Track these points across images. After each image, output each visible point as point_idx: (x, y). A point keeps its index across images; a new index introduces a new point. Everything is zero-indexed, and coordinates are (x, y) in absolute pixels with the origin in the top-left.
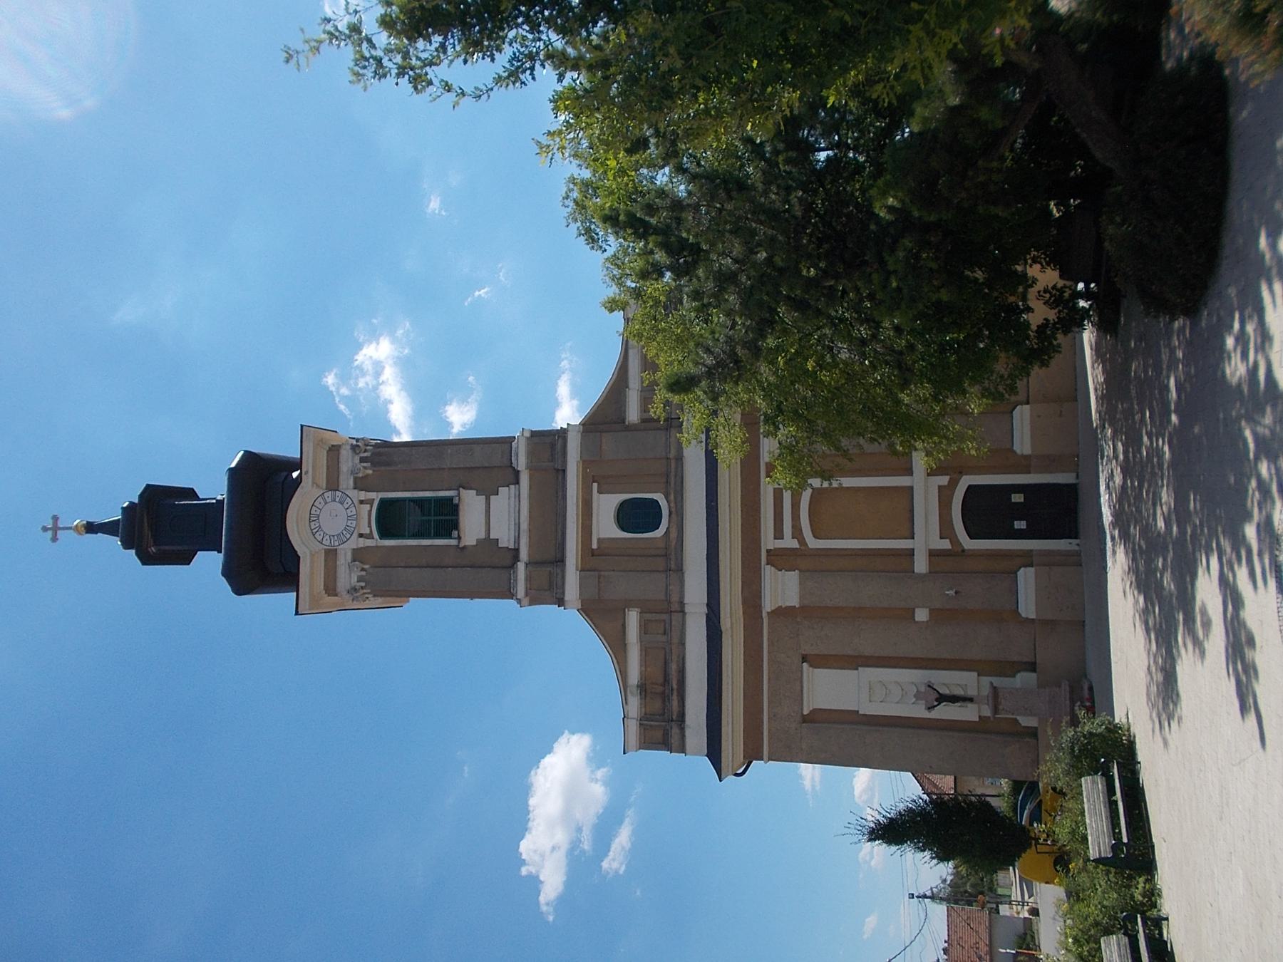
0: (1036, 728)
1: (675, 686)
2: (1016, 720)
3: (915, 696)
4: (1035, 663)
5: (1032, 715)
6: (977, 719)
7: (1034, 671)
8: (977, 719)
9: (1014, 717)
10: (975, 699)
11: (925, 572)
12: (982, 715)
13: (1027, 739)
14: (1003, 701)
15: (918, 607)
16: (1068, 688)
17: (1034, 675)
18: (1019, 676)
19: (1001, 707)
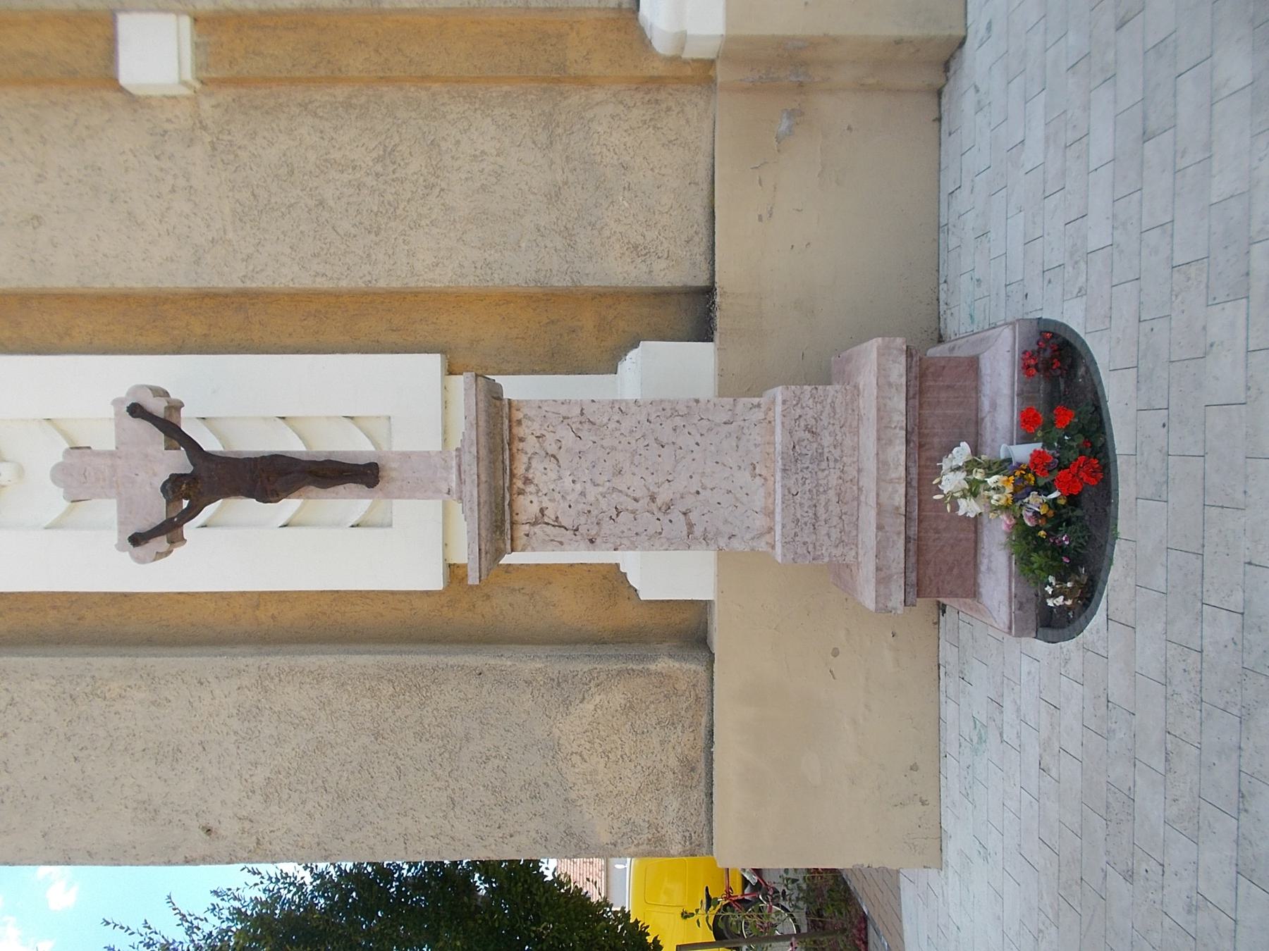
0: (703, 607)
1: (1013, 599)
2: (614, 578)
3: (62, 474)
4: (708, 292)
5: (691, 536)
6: (434, 580)
7: (704, 332)
8: (434, 580)
9: (600, 556)
10: (391, 469)
11: (441, 589)
12: (693, 667)
13: (664, 664)
14: (537, 472)
15: (126, 10)
16: (898, 371)
17: (701, 354)
18: (632, 362)
19: (527, 506)
